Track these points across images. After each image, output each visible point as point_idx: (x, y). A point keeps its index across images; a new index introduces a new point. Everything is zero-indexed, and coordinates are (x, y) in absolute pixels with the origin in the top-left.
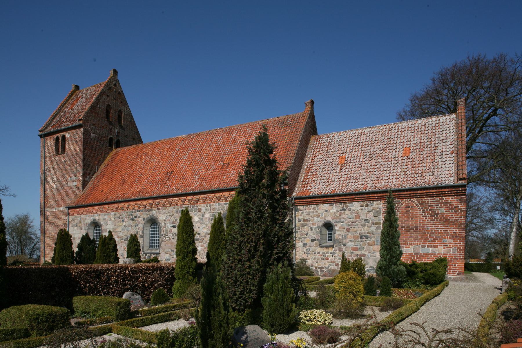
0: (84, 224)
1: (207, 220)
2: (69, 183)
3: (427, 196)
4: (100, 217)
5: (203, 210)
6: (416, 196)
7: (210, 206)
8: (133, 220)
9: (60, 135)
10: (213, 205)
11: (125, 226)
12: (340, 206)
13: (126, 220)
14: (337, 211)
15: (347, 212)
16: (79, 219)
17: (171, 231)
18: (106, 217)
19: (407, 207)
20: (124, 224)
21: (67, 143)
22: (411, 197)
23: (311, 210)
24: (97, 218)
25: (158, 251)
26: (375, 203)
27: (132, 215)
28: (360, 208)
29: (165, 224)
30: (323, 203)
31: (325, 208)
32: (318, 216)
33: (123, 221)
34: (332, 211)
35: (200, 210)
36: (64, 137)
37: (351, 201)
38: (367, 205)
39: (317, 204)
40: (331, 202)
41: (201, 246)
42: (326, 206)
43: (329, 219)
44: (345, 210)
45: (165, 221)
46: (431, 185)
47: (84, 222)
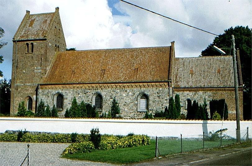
0: (51, 94)
1: (130, 96)
2: (35, 70)
3: (229, 90)
4: (63, 91)
5: (128, 91)
6: (225, 90)
7: (132, 89)
8: (86, 94)
9: (29, 43)
10: (133, 89)
11: (80, 97)
12: (194, 93)
13: (81, 93)
14: (193, 94)
15: (197, 95)
16: (47, 91)
17: (109, 100)
18: (67, 91)
19: (221, 94)
20: (80, 95)
21: (21, 21)
22: (222, 90)
23: (181, 94)
24: (60, 91)
25: (101, 110)
26: (209, 92)
27: (85, 91)
28: (202, 94)
29: (106, 97)
30: (186, 91)
31: (187, 93)
32: (184, 96)
33: (79, 94)
34: (190, 94)
35: (126, 91)
36: (32, 44)
37: (199, 91)
38: (205, 93)
39: (183, 91)
40: (190, 91)
41: (127, 108)
42: (188, 92)
43: (189, 98)
44: (196, 94)
45: (106, 95)
46: (128, 82)
47: (51, 93)
